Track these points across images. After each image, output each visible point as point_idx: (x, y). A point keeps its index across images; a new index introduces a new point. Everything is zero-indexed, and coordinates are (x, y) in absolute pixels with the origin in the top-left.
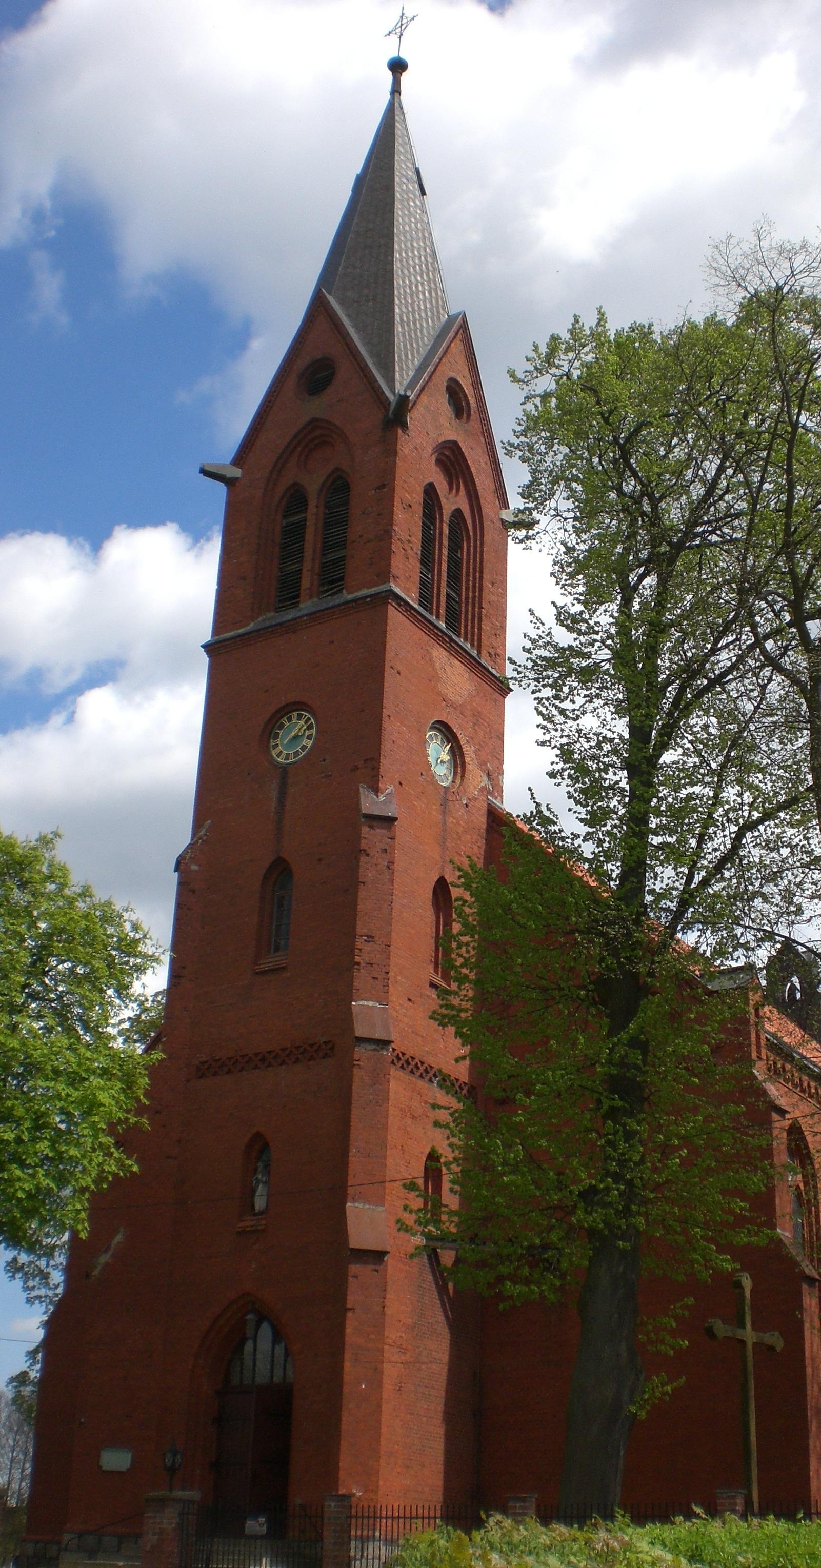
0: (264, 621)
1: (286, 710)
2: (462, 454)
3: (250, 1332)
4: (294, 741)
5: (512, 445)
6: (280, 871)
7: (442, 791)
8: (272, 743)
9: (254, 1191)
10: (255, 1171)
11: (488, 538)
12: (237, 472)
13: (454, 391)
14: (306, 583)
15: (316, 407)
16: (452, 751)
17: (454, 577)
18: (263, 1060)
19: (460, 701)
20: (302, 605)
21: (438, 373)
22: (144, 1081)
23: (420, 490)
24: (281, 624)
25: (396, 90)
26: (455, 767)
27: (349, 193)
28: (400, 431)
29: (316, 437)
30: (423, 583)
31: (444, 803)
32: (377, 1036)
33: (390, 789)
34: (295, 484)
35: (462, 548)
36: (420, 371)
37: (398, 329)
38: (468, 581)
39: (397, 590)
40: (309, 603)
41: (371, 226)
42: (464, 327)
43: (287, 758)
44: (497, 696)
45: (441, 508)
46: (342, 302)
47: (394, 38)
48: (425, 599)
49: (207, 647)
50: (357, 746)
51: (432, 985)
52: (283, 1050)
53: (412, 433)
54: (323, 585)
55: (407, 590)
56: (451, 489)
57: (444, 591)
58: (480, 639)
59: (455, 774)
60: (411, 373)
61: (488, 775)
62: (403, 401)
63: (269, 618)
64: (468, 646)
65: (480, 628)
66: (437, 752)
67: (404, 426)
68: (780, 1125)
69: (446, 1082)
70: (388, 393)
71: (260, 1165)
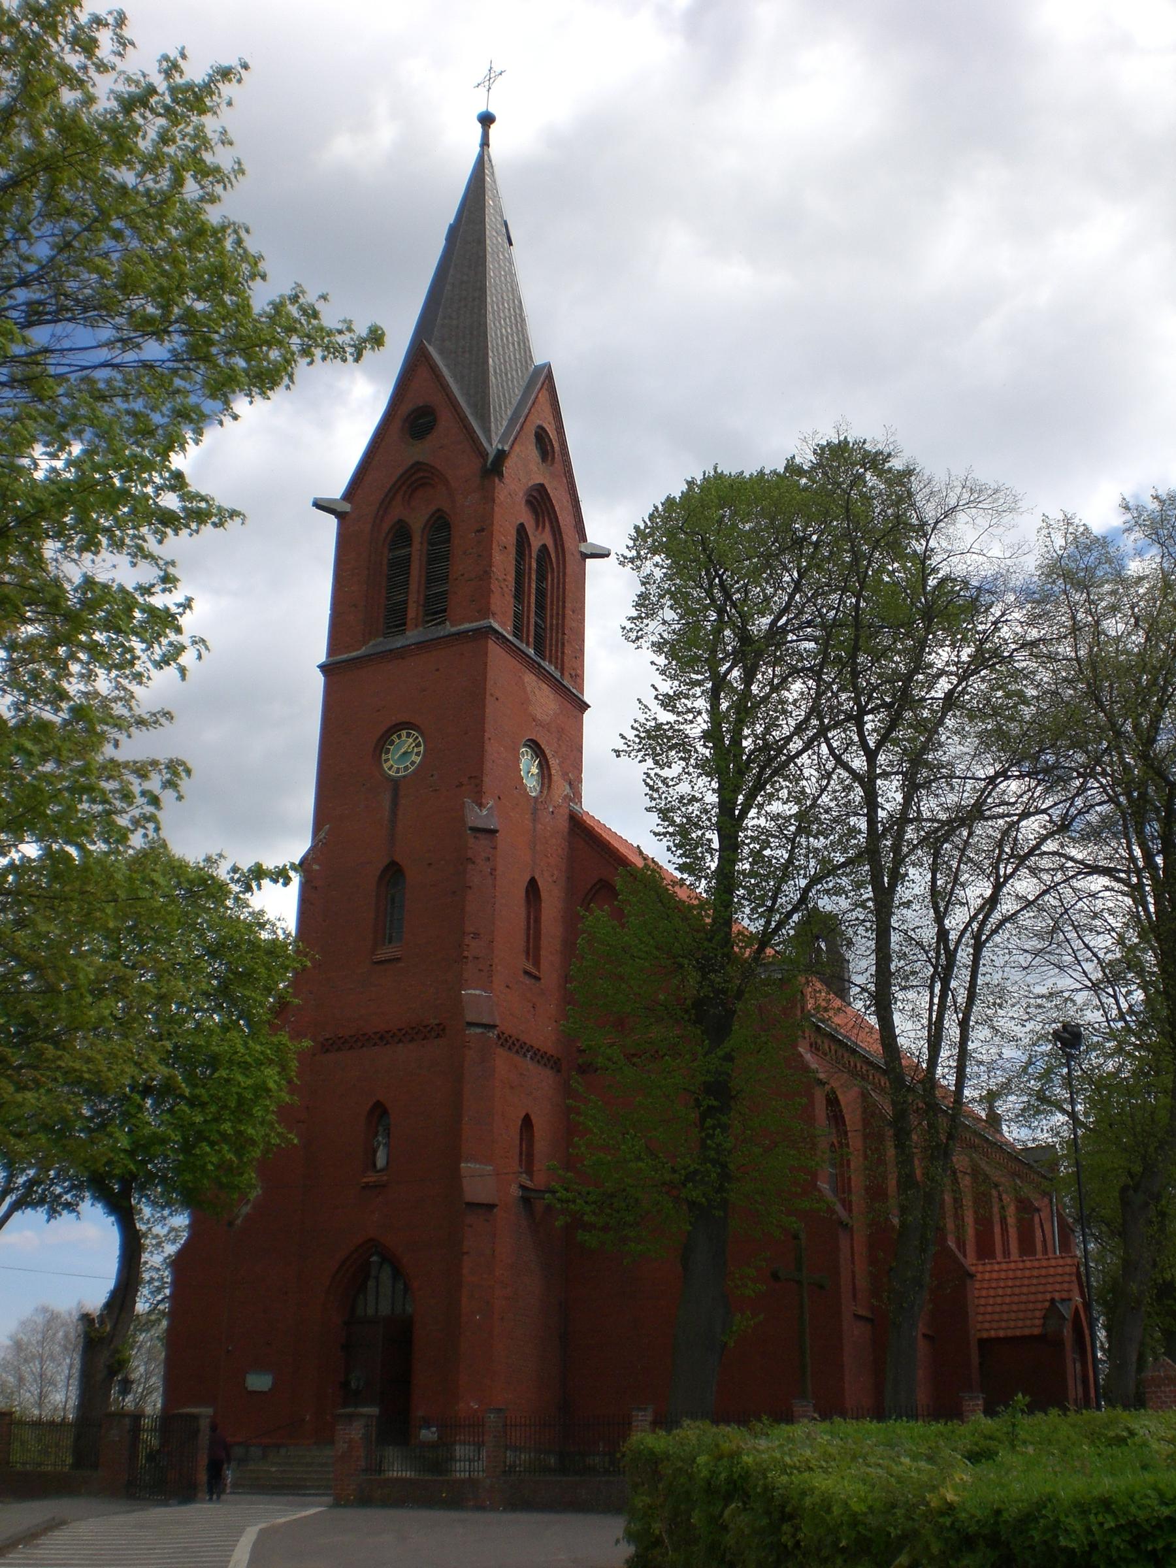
0: (374, 645)
1: (397, 728)
2: (548, 495)
3: (373, 1273)
4: (404, 756)
5: (625, 558)
6: (393, 873)
7: (532, 802)
8: (384, 757)
9: (375, 1152)
10: (376, 1135)
11: (569, 571)
12: (347, 507)
13: (541, 437)
14: (411, 614)
15: (419, 452)
16: (540, 766)
17: (541, 606)
18: (382, 1038)
19: (548, 719)
20: (408, 633)
21: (527, 423)
22: (294, 1064)
23: (514, 532)
24: (391, 651)
25: (485, 143)
26: (543, 778)
27: (442, 243)
28: (497, 480)
29: (418, 479)
30: (516, 615)
31: (535, 812)
32: (485, 1021)
33: (491, 803)
34: (400, 521)
35: (546, 579)
36: (513, 420)
37: (492, 379)
38: (552, 609)
39: (496, 626)
40: (415, 632)
41: (465, 278)
42: (550, 377)
43: (398, 771)
44: (577, 713)
45: (530, 545)
46: (441, 352)
47: (483, 90)
48: (518, 631)
49: (323, 668)
50: (463, 761)
51: (526, 973)
52: (400, 1030)
53: (506, 481)
54: (427, 615)
55: (503, 625)
56: (537, 526)
57: (532, 621)
58: (563, 661)
59: (543, 785)
60: (505, 423)
61: (570, 784)
62: (501, 456)
63: (378, 644)
64: (551, 669)
65: (563, 653)
66: (528, 767)
67: (501, 475)
68: (819, 1095)
69: (540, 1057)
70: (486, 444)
71: (381, 1129)
